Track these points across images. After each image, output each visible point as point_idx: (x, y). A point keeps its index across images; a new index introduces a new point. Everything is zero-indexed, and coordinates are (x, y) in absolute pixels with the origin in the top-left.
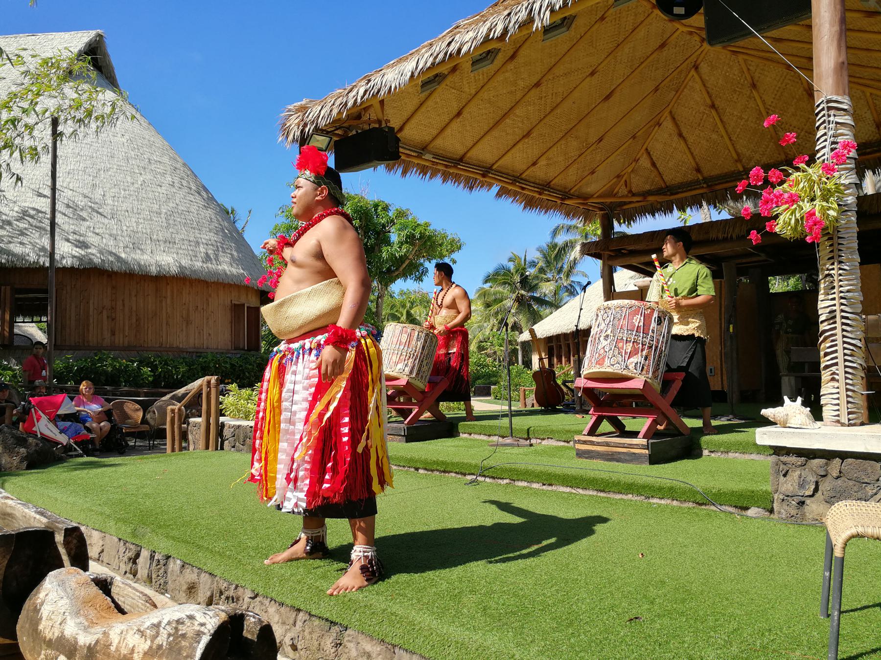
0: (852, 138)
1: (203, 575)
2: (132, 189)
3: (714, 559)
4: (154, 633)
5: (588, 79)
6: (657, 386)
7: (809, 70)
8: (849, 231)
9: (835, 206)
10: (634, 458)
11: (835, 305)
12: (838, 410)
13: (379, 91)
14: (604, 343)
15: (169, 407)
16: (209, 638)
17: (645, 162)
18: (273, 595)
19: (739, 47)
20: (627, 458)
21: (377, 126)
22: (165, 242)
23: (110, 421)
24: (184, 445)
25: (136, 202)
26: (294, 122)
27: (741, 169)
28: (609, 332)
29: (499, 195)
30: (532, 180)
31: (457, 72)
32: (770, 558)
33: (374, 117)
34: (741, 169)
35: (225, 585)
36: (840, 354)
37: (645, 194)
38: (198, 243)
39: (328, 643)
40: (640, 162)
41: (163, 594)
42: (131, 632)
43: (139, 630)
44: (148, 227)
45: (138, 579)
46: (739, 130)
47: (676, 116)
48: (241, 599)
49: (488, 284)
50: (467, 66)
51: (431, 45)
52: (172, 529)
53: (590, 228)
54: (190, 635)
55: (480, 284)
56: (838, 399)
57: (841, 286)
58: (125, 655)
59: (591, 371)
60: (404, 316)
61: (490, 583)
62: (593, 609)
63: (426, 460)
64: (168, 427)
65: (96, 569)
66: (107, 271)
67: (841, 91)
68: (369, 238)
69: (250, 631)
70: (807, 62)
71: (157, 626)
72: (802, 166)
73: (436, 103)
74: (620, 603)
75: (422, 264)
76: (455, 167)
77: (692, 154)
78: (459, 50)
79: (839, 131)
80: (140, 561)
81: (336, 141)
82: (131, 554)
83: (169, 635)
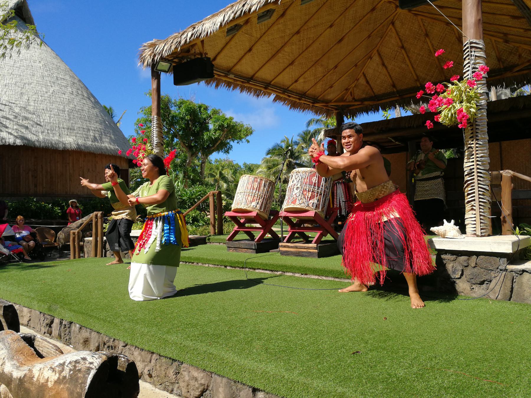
0: (484, 65)
1: (93, 333)
2: (46, 95)
3: (402, 316)
4: (60, 369)
5: (328, 30)
6: (323, 215)
7: (460, 26)
8: (482, 121)
9: (475, 106)
10: (310, 255)
11: (473, 165)
12: (475, 227)
13: (200, 34)
14: (296, 191)
15: (72, 231)
16: (95, 371)
17: (362, 81)
18: (137, 344)
19: (418, 11)
20: (307, 254)
21: (200, 57)
22: (68, 129)
23: (35, 240)
24: (81, 255)
25: (49, 104)
26: (147, 53)
27: (419, 86)
28: (299, 186)
29: (275, 100)
30: (295, 91)
31: (249, 24)
32: (436, 315)
33: (197, 51)
34: (419, 86)
35: (107, 339)
36: (476, 194)
37: (362, 100)
38: (89, 130)
39: (171, 372)
40: (360, 81)
41: (68, 345)
42: (46, 369)
43: (51, 368)
44: (57, 119)
45: (53, 337)
46: (418, 62)
47: (381, 53)
48: (117, 347)
49: (269, 156)
50: (255, 20)
51: (232, 6)
52: (74, 306)
53: (330, 121)
54: (83, 370)
55: (264, 156)
56: (475, 221)
57: (477, 154)
58: (42, 383)
59: (289, 207)
60: (218, 175)
61: (270, 334)
62: (332, 347)
63: (231, 261)
64: (71, 243)
65: (24, 330)
66: (31, 147)
67: (478, 37)
68: (196, 127)
69: (122, 365)
70: (459, 20)
71: (63, 365)
72: (456, 81)
73: (236, 43)
74: (348, 344)
75: (228, 143)
76: (248, 83)
77: (390, 76)
78: (250, 9)
79: (477, 61)
80: (54, 325)
81: (174, 66)
82: (48, 321)
83: (70, 370)
